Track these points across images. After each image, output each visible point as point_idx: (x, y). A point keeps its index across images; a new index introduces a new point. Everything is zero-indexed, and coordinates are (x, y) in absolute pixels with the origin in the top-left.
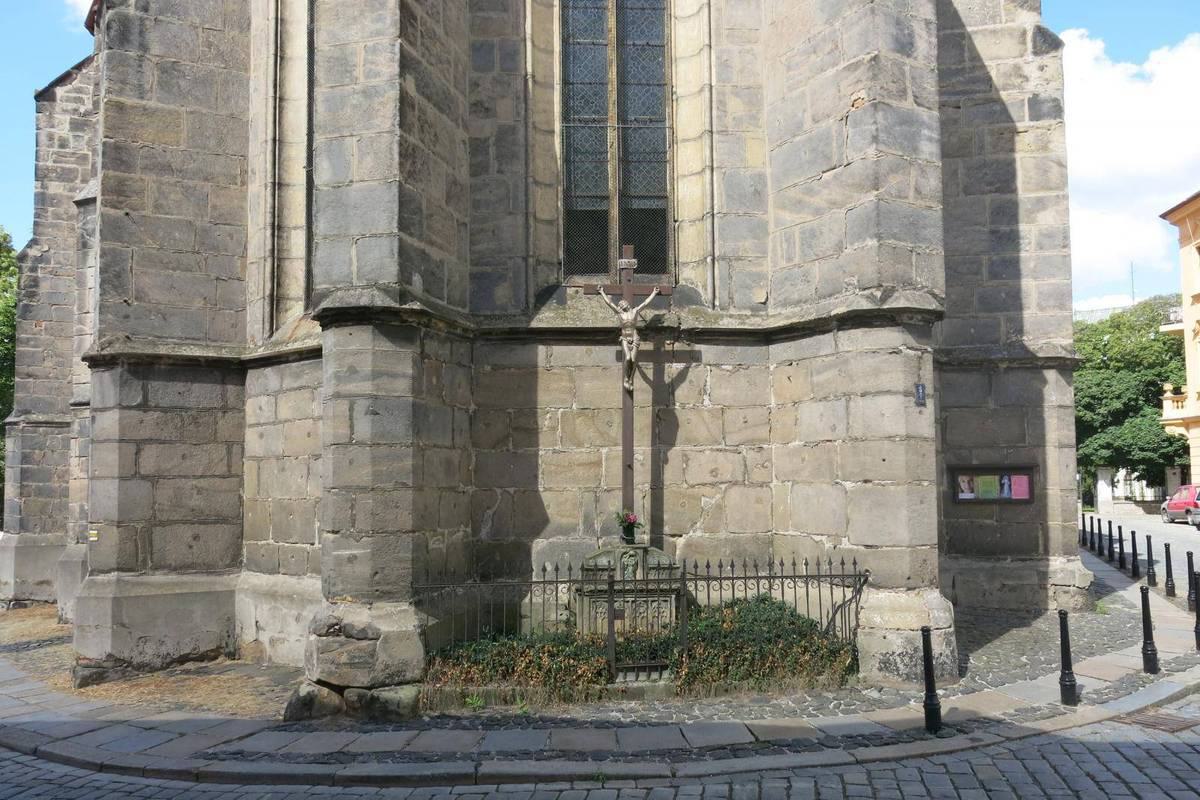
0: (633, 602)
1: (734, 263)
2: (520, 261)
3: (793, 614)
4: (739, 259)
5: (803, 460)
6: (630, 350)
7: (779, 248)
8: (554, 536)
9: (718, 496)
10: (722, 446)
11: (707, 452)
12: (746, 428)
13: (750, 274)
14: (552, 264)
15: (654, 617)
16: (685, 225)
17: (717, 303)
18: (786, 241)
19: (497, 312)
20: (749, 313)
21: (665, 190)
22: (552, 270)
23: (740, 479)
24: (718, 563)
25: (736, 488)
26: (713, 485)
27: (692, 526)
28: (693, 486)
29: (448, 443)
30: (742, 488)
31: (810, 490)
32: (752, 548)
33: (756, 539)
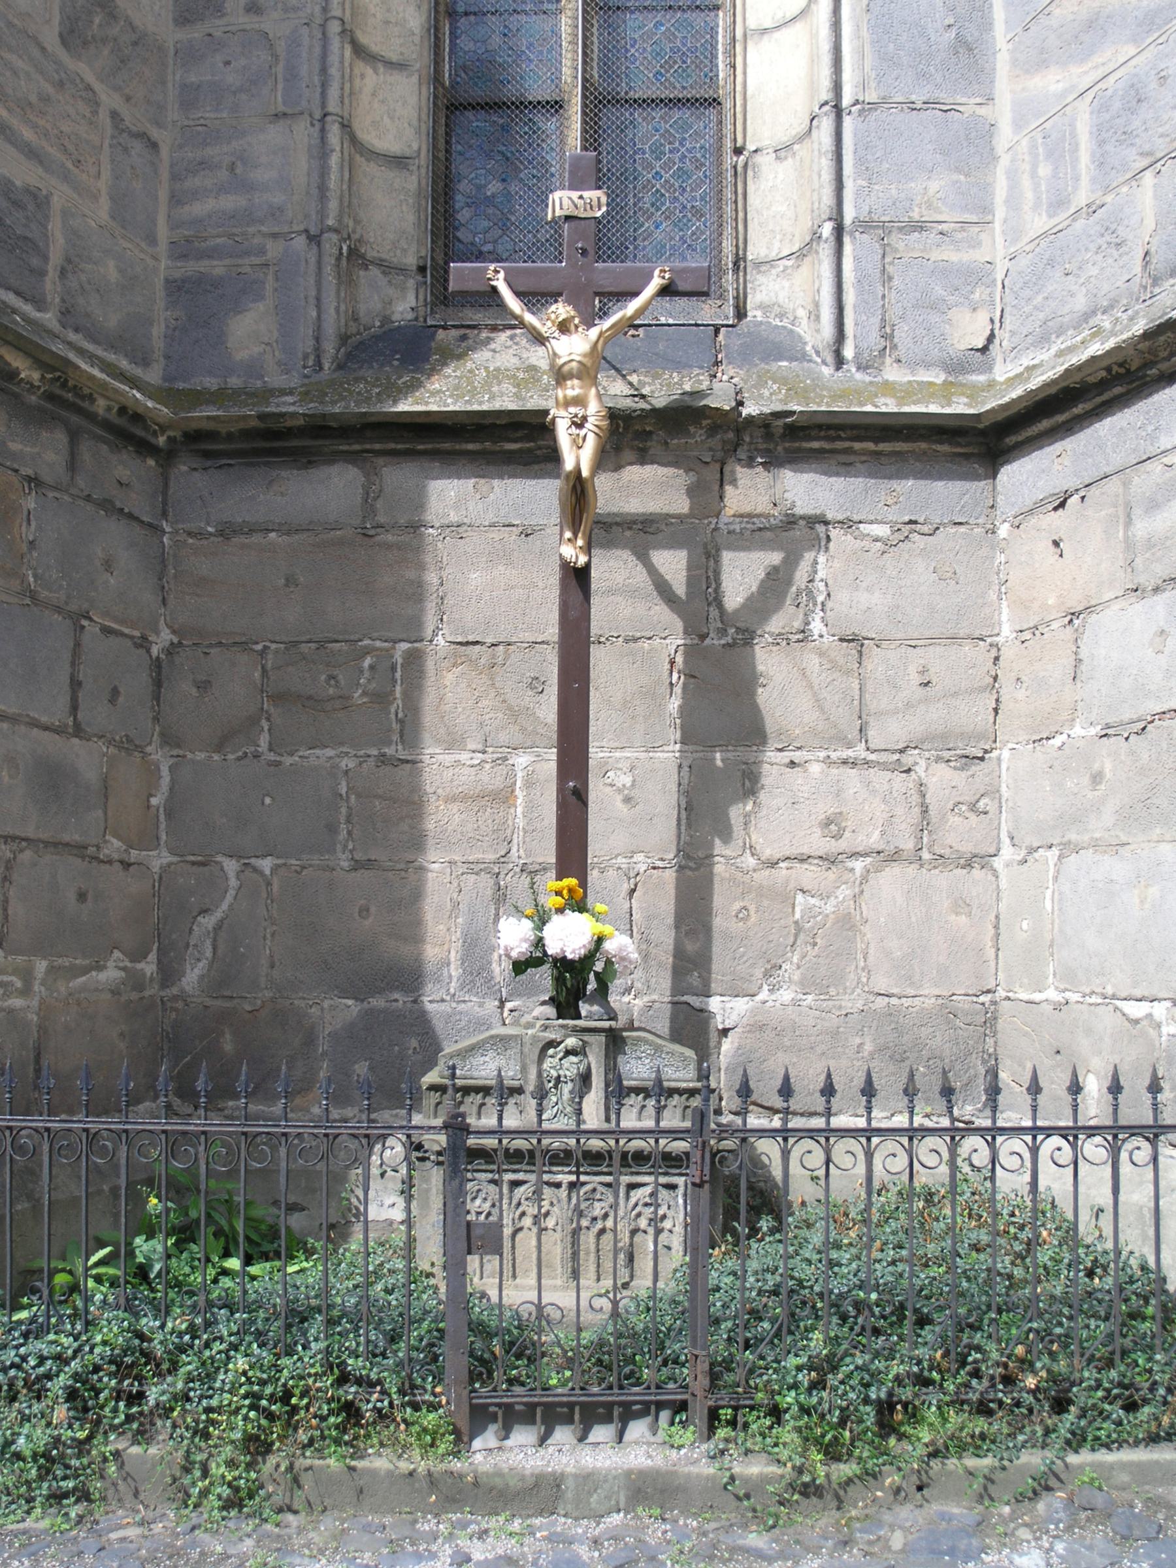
0: (572, 1186)
1: (898, 241)
2: (300, 242)
3: (1070, 1234)
4: (919, 227)
5: (1097, 778)
6: (578, 445)
7: (1026, 183)
8: (380, 991)
9: (844, 892)
10: (859, 751)
11: (815, 769)
12: (926, 700)
13: (944, 271)
14: (402, 270)
15: (634, 1232)
16: (765, 161)
17: (848, 352)
18: (1050, 154)
19: (234, 382)
20: (937, 377)
21: (714, 79)
22: (404, 289)
23: (909, 845)
24: (859, 1081)
25: (894, 871)
26: (830, 860)
27: (767, 974)
28: (773, 864)
29: (58, 713)
30: (912, 870)
31: (1115, 868)
32: (939, 1040)
33: (948, 1012)
